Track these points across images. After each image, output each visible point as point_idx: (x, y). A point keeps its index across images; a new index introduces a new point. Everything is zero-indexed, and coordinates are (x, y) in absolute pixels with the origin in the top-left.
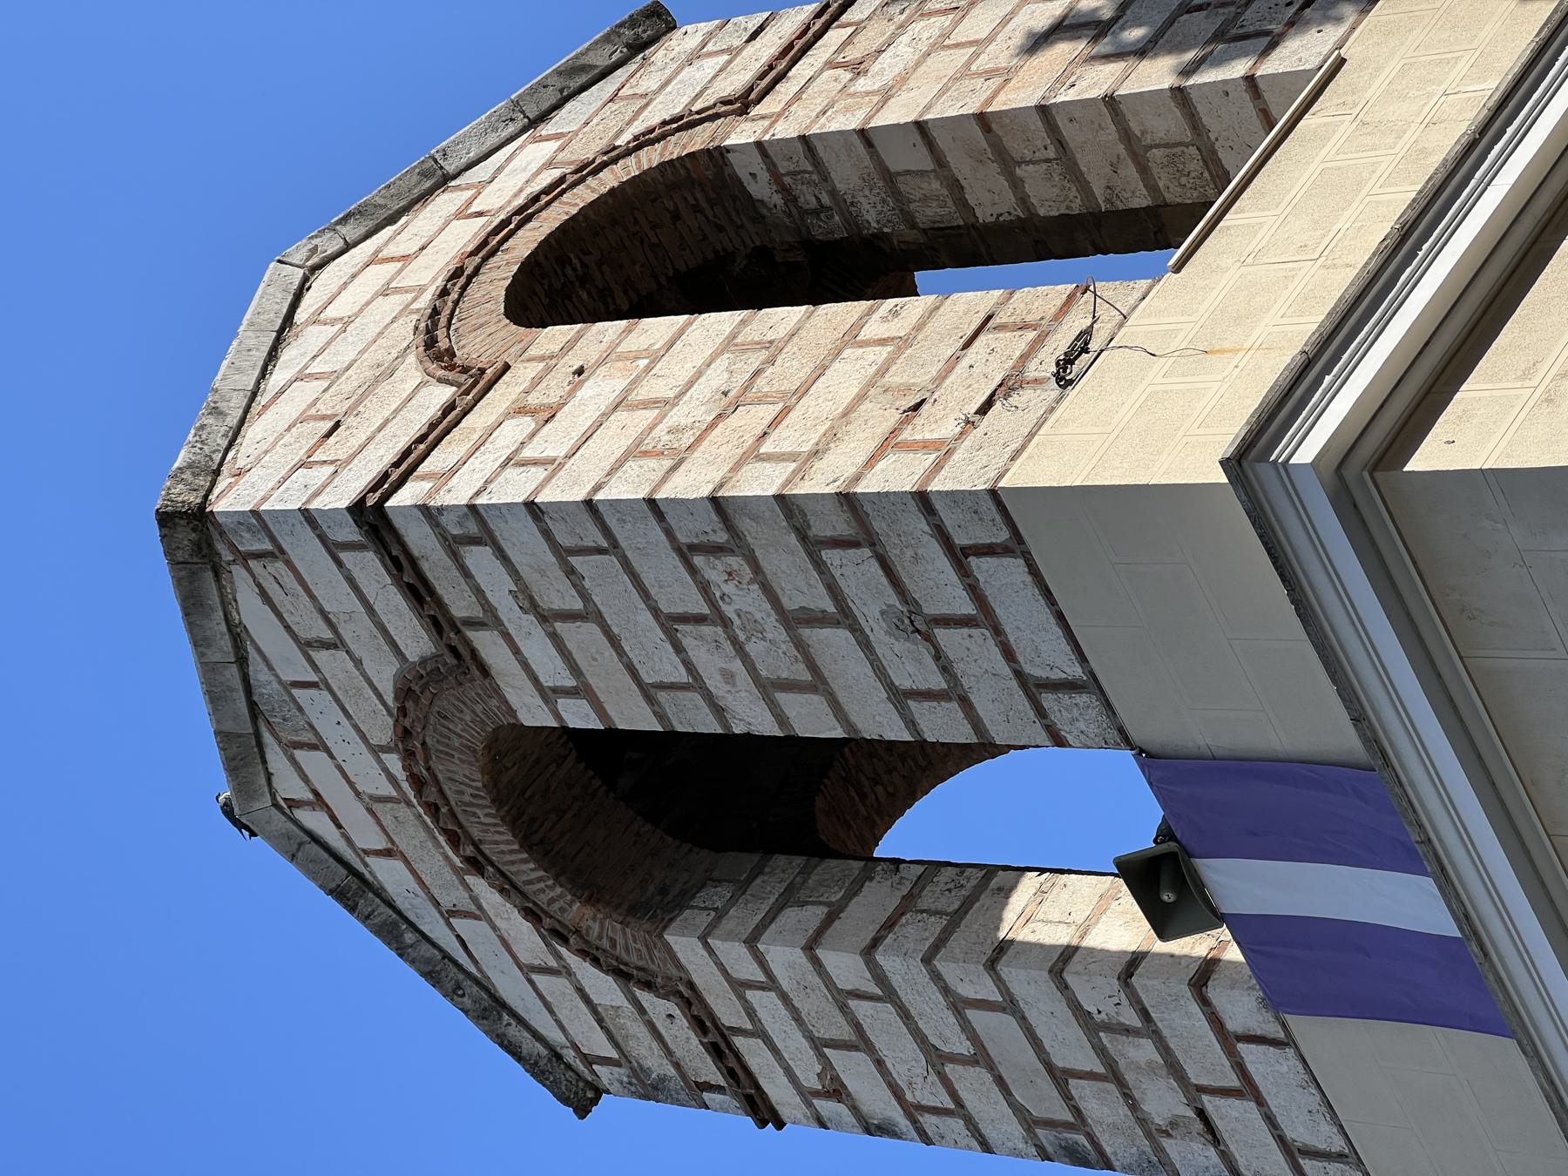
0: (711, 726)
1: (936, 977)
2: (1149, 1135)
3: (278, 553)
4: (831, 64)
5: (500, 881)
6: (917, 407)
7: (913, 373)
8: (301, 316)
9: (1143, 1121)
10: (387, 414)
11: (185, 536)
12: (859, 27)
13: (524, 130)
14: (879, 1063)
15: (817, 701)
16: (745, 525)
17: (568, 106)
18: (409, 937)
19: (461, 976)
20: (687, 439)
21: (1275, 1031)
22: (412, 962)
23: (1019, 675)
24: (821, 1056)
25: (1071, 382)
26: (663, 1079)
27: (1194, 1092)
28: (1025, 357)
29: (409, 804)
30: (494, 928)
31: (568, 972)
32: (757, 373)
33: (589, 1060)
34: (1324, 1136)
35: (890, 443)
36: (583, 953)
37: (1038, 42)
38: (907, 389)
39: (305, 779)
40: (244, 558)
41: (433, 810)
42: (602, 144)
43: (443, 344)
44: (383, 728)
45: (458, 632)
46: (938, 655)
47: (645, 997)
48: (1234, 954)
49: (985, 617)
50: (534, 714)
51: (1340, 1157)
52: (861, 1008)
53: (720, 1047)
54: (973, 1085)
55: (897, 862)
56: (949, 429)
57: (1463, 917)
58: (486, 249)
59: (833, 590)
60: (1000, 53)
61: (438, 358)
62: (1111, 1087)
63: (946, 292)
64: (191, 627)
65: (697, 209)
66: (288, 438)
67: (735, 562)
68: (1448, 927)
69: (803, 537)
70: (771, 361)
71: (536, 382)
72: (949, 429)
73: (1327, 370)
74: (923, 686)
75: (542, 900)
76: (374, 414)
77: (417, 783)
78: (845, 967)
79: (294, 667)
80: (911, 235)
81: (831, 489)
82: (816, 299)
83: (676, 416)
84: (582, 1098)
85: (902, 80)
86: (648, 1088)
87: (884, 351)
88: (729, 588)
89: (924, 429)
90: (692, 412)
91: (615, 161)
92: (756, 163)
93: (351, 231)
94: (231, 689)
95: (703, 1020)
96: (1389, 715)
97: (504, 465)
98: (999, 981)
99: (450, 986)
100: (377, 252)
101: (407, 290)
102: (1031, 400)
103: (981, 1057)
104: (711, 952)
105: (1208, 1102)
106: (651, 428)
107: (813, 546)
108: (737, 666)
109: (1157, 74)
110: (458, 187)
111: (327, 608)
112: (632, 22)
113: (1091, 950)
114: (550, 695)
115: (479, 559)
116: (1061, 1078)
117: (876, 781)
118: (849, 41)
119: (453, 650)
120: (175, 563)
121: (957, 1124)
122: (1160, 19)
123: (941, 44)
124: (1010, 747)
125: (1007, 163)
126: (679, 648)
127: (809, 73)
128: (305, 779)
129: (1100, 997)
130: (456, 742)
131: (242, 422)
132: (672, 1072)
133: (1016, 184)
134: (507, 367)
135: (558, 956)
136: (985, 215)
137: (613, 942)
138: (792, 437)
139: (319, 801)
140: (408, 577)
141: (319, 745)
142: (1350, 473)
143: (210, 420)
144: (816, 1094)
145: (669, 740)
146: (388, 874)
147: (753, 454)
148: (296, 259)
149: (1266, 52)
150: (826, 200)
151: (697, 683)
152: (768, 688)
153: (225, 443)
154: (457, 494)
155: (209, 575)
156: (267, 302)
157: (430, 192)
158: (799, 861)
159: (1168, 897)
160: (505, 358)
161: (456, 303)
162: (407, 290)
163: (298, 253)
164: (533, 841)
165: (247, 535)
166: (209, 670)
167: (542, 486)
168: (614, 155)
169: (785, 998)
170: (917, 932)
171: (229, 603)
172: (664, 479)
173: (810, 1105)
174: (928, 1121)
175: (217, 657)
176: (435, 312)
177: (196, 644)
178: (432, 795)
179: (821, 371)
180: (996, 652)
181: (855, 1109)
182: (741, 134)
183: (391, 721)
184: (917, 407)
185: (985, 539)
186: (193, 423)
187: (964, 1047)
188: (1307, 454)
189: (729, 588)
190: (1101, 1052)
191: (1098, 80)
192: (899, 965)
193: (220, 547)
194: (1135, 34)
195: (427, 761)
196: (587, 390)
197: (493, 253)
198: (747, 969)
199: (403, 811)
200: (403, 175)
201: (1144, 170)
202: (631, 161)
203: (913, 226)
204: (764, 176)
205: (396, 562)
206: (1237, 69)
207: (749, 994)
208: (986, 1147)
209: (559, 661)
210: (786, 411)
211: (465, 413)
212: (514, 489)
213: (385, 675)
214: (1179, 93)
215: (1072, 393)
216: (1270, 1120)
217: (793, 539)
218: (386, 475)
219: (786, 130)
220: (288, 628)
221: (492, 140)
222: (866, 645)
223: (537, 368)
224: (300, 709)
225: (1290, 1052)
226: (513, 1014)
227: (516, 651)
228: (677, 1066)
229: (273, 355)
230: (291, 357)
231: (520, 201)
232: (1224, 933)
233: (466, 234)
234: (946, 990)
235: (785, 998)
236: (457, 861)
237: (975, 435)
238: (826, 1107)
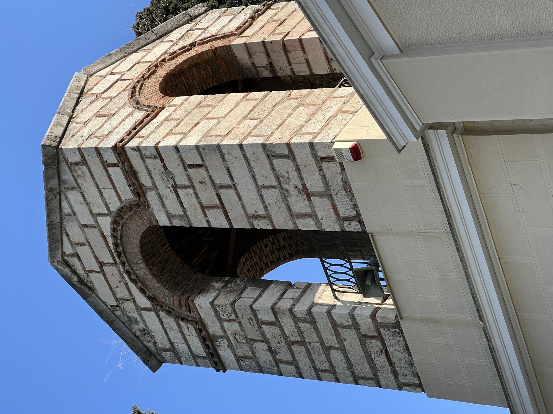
110: (273, 9)
154: (150, 142)
167: (100, 143)
225: (362, 333)
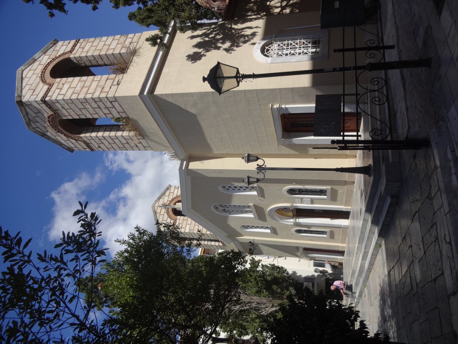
4: (79, 48)
6: (103, 88)
10: (40, 89)
12: (81, 43)
14: (104, 145)
17: (48, 51)
18: (50, 139)
25: (119, 84)
46: (109, 110)
49: (114, 107)
61: (44, 82)
79: (34, 115)
83: (77, 89)
90: (78, 89)
100: (30, 69)
118: (81, 45)
127: (77, 49)
134: (54, 84)
139: (38, 127)
141: (38, 122)
145: (80, 120)
147: (87, 93)
150: (82, 62)
169: (94, 140)
171: (25, 110)
184: (103, 88)
196: (65, 86)
197: (46, 69)
199: (49, 127)
201: (117, 60)
215: (119, 86)
221: (40, 55)
222: (102, 110)
223: (57, 84)
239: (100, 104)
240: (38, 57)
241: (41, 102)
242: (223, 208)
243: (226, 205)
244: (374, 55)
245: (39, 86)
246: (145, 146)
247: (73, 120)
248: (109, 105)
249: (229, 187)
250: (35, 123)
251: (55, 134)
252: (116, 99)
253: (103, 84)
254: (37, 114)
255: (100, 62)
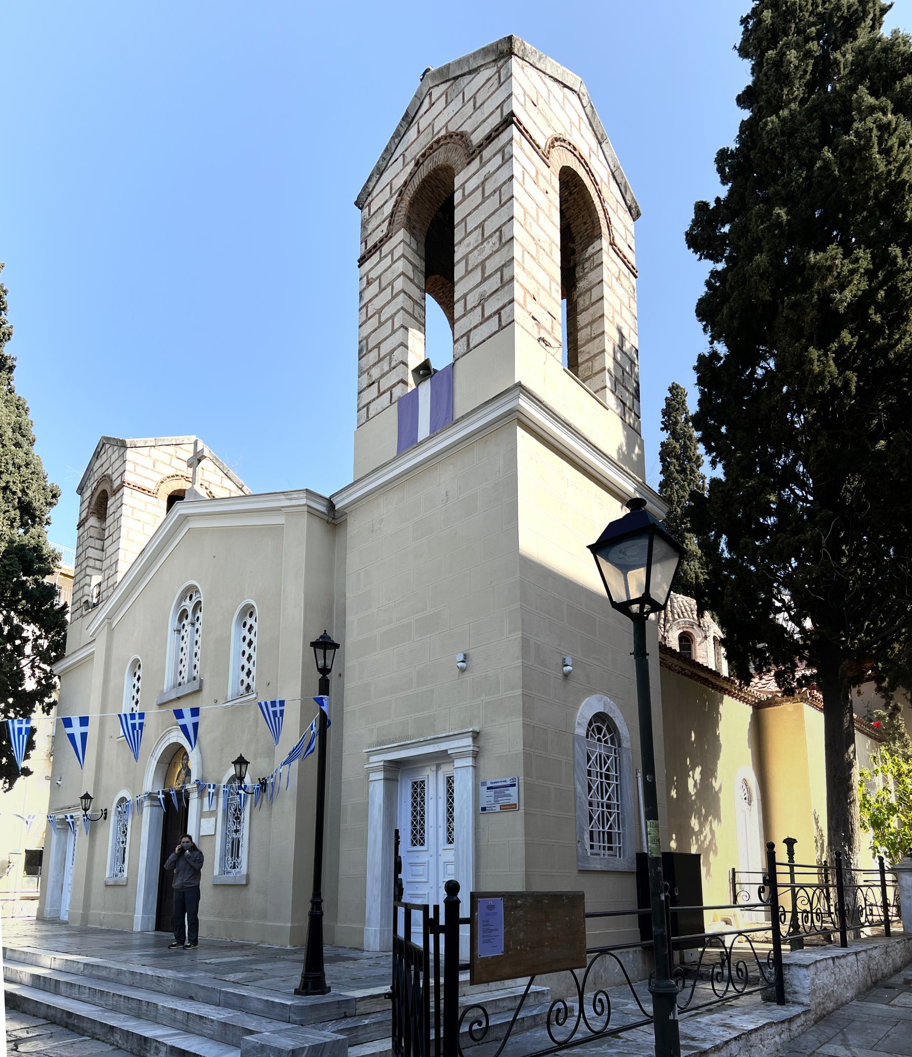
0: (456, 240)
1: (398, 311)
2: (367, 370)
3: (500, 85)
4: (620, 270)
5: (413, 172)
7: (543, 298)
8: (566, 89)
9: (370, 368)
11: (505, 47)
12: (628, 279)
13: (611, 171)
14: (377, 295)
15: (463, 272)
16: (507, 247)
19: (387, 160)
20: (528, 229)
21: (393, 400)
22: (390, 142)
23: (470, 330)
24: (377, 278)
26: (367, 229)
27: (378, 381)
28: (545, 329)
29: (432, 138)
30: (401, 171)
31: (391, 197)
32: (544, 250)
33: (369, 205)
34: (372, 413)
35: (526, 291)
36: (396, 202)
37: (620, 331)
38: (539, 296)
39: (437, 99)
40: (499, 72)
41: (431, 148)
42: (605, 198)
43: (556, 144)
44: (452, 128)
45: (479, 153)
46: (475, 307)
47: (387, 222)
48: (410, 390)
49: (485, 320)
50: (458, 181)
51: (368, 417)
52: (389, 289)
53: (376, 247)
54: (374, 323)
55: (424, 299)
56: (529, 308)
57: (422, 443)
58: (580, 159)
59: (490, 276)
60: (618, 320)
61: (552, 143)
62: (377, 360)
63: (561, 307)
64: (479, 51)
65: (587, 230)
66: (532, 86)
67: (497, 245)
68: (419, 439)
69: (503, 266)
70: (547, 255)
71: (545, 177)
72: (529, 308)
73: (540, 407)
74: (468, 303)
75: (409, 187)
76: (539, 119)
77: (438, 141)
78: (399, 284)
79: (468, 95)
80: (575, 297)
81: (515, 274)
82: (562, 268)
83: (534, 224)
84: (359, 204)
85: (614, 292)
86: (364, 226)
87: (548, 288)
88: (491, 244)
89: (529, 300)
90: (536, 231)
91: (601, 202)
92: (597, 248)
93: (588, 109)
94: (462, 69)
95: (383, 241)
96: (465, 424)
97: (523, 167)
98: (399, 328)
99: (384, 156)
101: (571, 130)
102: (534, 331)
103: (381, 324)
104: (400, 243)
105: (376, 384)
106: (531, 217)
107: (501, 269)
108: (472, 247)
109: (609, 363)
111: (485, 104)
112: (637, 207)
113: (407, 353)
114: (463, 186)
115: (499, 158)
116: (378, 346)
117: (443, 293)
118: (625, 276)
119: (474, 152)
120: (498, 43)
121: (364, 318)
122: (622, 364)
123: (622, 303)
124: (453, 331)
125: (591, 323)
126: (475, 229)
128: (437, 99)
129: (398, 356)
130: (449, 155)
131: (537, 69)
132: (369, 232)
133: (586, 326)
134: (549, 167)
135: (395, 193)
136: (579, 318)
137: (400, 212)
138: (529, 263)
140: (494, 134)
141: (447, 104)
142: (517, 413)
143: (538, 56)
144: (368, 277)
145: (451, 227)
146: (412, 133)
147: (524, 250)
148: (582, 88)
149: (611, 390)
150: (586, 270)
151: (467, 235)
152: (466, 257)
153: (531, 62)
154: (516, 151)
155: (494, 58)
156: (572, 79)
157: (597, 138)
158: (424, 270)
159: (421, 372)
160: (551, 166)
161: (567, 148)
162: (571, 130)
163: (584, 90)
164: (425, 182)
165: (505, 72)
166: (466, 60)
167: (518, 181)
168: (602, 201)
169: (390, 267)
170: (409, 305)
172: (518, 221)
173: (365, 275)
174: (364, 310)
175: (471, 63)
176: (565, 141)
177: (474, 54)
178: (435, 147)
179: (544, 270)
180: (476, 324)
181: (365, 289)
182: (605, 243)
183: (454, 130)
185: (503, 319)
186: (537, 49)
187: (383, 320)
188: (521, 402)
189: (491, 244)
190: (385, 357)
191: (609, 348)
192: (401, 300)
193: (502, 61)
194: (619, 356)
195: (444, 144)
197: (580, 161)
198: (397, 254)
199: (431, 136)
200: (602, 129)
201: (587, 360)
202: (601, 208)
203: (578, 297)
204: (593, 251)
205: (498, 129)
206: (608, 384)
207: (390, 255)
208: (360, 326)
209: (472, 189)
210: (535, 260)
211: (537, 153)
212: (517, 171)
213: (467, 128)
214: (604, 369)
216: (374, 400)
217: (503, 263)
218: (521, 124)
219: (605, 258)
220: (479, 89)
221: (610, 160)
222: (477, 286)
224: (457, 96)
226: (379, 178)
227: (474, 174)
228: (370, 234)
229: (556, 80)
230: (554, 86)
231: (593, 170)
232: (414, 387)
233: (584, 152)
234: (395, 314)
235: (390, 267)
236: (418, 157)
237: (527, 315)
238: (365, 279)
239: (494, 283)
240: (606, 153)
241: (506, 112)
242: (190, 612)
243: (200, 620)
244: (742, 963)
245: (545, 122)
246: (372, 406)
247: (448, 207)
248: (491, 307)
249: (251, 627)
250: (444, 96)
251: (409, 155)
252: (506, 325)
253: (543, 303)
254: (471, 102)
255: (583, 319)
